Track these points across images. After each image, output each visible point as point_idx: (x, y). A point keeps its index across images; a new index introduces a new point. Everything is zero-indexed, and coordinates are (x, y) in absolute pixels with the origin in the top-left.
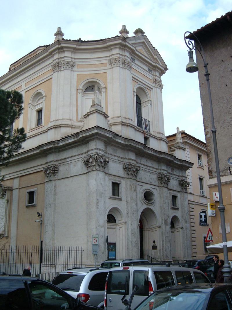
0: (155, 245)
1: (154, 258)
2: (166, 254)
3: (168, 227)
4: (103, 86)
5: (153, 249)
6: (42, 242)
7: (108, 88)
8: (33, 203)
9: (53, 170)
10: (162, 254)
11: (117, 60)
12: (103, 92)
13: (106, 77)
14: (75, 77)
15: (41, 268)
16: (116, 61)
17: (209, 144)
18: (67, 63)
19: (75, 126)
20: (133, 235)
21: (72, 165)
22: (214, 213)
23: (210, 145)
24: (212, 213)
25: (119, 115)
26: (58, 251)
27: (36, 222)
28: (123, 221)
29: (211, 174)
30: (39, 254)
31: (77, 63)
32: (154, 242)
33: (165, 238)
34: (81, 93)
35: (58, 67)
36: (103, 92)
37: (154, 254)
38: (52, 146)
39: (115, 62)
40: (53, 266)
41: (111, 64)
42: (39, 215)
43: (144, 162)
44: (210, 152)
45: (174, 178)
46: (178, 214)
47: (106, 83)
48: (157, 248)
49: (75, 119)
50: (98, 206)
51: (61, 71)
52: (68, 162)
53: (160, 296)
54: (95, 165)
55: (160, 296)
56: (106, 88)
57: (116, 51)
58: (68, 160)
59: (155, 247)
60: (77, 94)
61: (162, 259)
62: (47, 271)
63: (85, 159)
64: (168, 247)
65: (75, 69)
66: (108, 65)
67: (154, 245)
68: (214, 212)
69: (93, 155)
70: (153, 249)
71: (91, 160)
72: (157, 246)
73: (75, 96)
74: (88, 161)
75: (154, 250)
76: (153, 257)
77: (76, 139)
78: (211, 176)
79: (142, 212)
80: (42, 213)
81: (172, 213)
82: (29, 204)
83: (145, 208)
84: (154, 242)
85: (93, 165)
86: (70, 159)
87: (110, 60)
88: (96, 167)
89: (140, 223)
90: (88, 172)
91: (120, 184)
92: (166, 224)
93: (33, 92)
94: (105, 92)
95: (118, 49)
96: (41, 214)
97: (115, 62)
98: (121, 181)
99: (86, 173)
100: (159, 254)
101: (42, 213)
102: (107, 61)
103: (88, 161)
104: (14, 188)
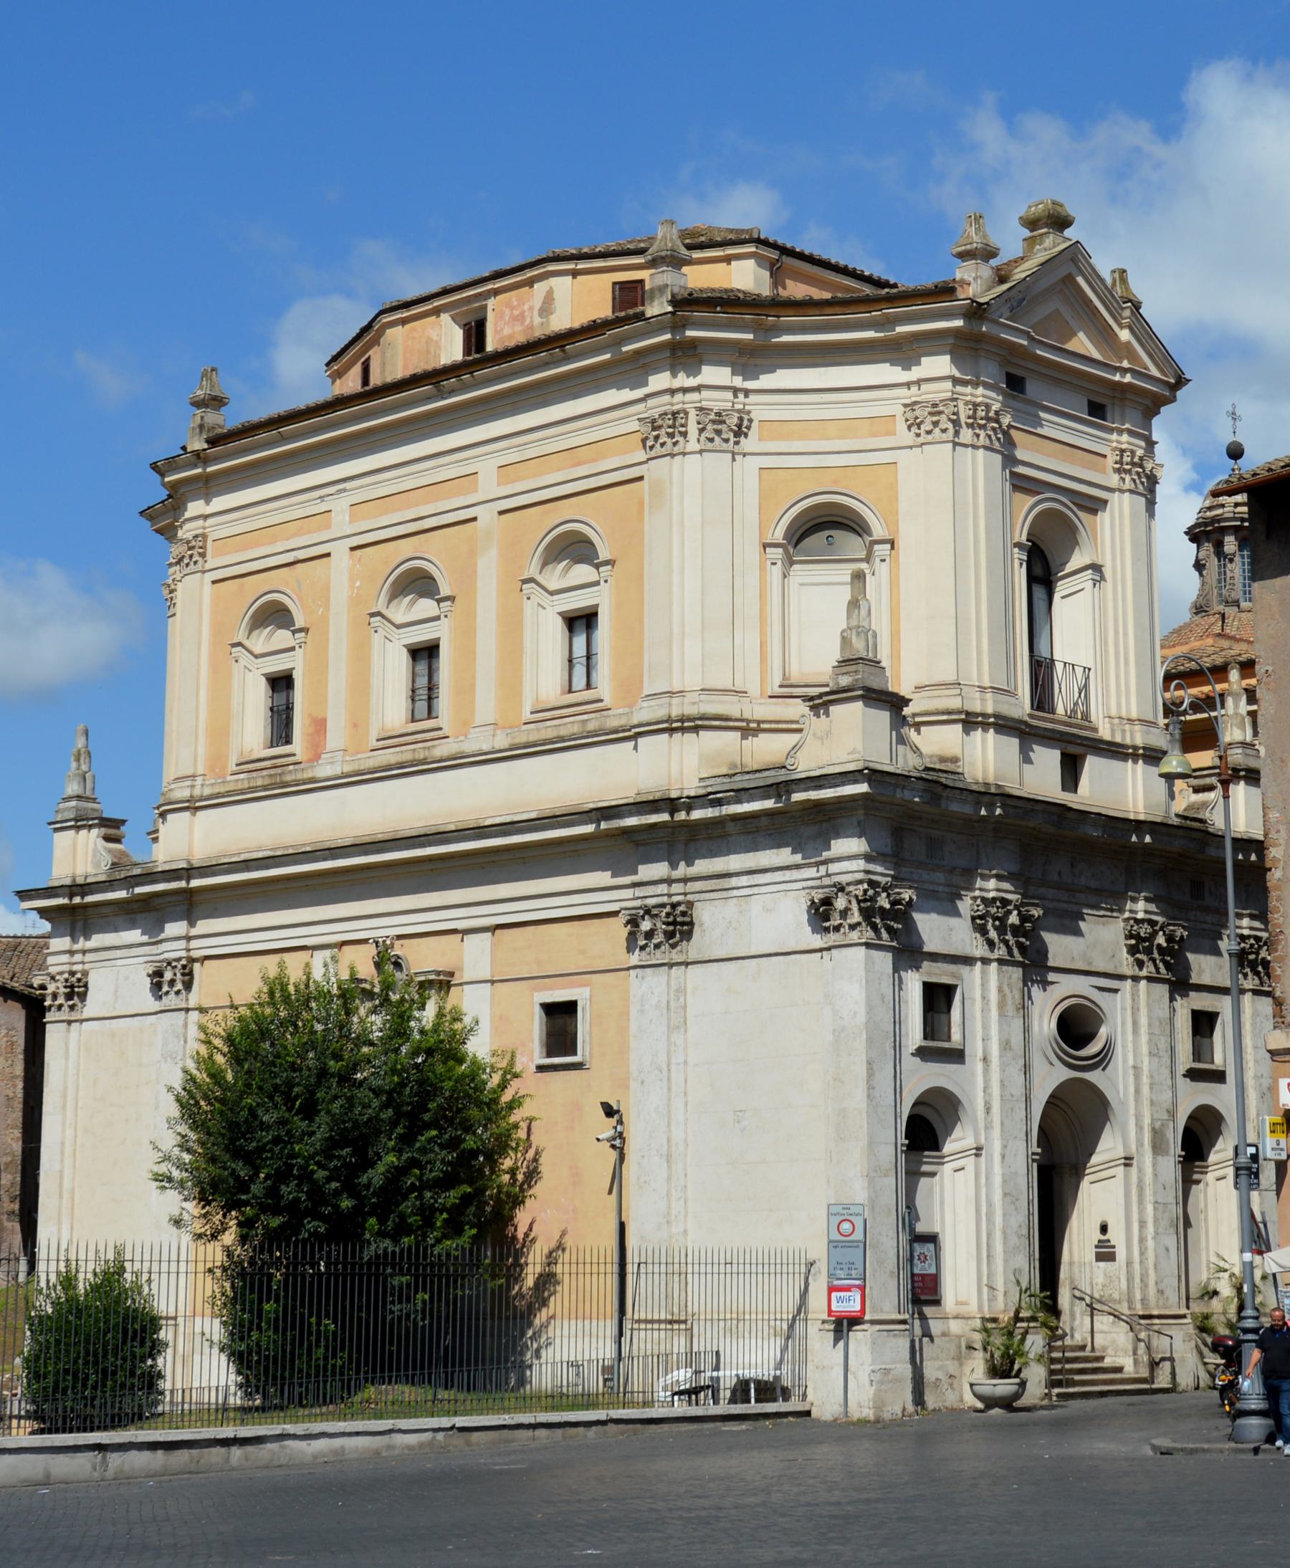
0: (1109, 1241)
1: (1104, 1299)
2: (1156, 1283)
3: (1170, 1166)
4: (878, 531)
5: (1100, 1257)
6: (622, 1227)
7: (939, 753)
8: (574, 1053)
9: (671, 919)
10: (1137, 1280)
11: (941, 408)
12: (878, 560)
13: (893, 487)
14: (752, 483)
15: (621, 1334)
16: (940, 413)
17: (1278, 905)
18: (712, 417)
19: (759, 722)
20: (1008, 1199)
21: (756, 905)
22: (1282, 1150)
23: (1282, 909)
24: (1273, 1149)
25: (951, 678)
26: (722, 1267)
27: (598, 1140)
28: (969, 1142)
29: (1281, 1011)
30: (616, 1277)
31: (760, 409)
32: (1104, 1229)
33: (1155, 1209)
34: (779, 563)
35: (671, 435)
36: (878, 560)
37: (1100, 1280)
38: (665, 817)
39: (935, 419)
40: (683, 1326)
41: (914, 424)
42: (609, 1111)
43: (1059, 874)
44: (1281, 932)
45: (1205, 926)
46: (1221, 1097)
47: (891, 517)
48: (1114, 1253)
49: (754, 687)
50: (873, 1088)
51: (684, 454)
52: (735, 893)
53: (464, 309)
54: (859, 924)
55: (464, 309)
56: (892, 543)
57: (939, 365)
58: (734, 882)
59: (1105, 1254)
60: (762, 568)
61: (1138, 1306)
62: (656, 1347)
63: (818, 897)
64: (1167, 1250)
65: (747, 444)
66: (901, 426)
67: (1101, 1244)
68: (1281, 1146)
69: (848, 884)
70: (1100, 1257)
71: (840, 903)
72: (1114, 1247)
73: (753, 578)
74: (827, 902)
75: (1102, 1264)
76: (1096, 1295)
77: (1071, 1377)
78: (1282, 1017)
79: (1052, 1096)
80: (618, 1101)
81: (1194, 1096)
82: (549, 1055)
83: (1062, 1080)
84: (1104, 1229)
85: (849, 921)
86: (744, 880)
87: (911, 406)
88: (861, 931)
89: (1038, 1147)
90: (829, 949)
91: (956, 986)
92: (1158, 1147)
93: (542, 525)
94: (888, 559)
95: (948, 357)
96: (615, 1108)
97: (935, 419)
98: (960, 978)
99: (821, 950)
100: (1124, 1286)
101: (618, 1101)
102: (893, 405)
103: (827, 902)
104: (466, 978)
